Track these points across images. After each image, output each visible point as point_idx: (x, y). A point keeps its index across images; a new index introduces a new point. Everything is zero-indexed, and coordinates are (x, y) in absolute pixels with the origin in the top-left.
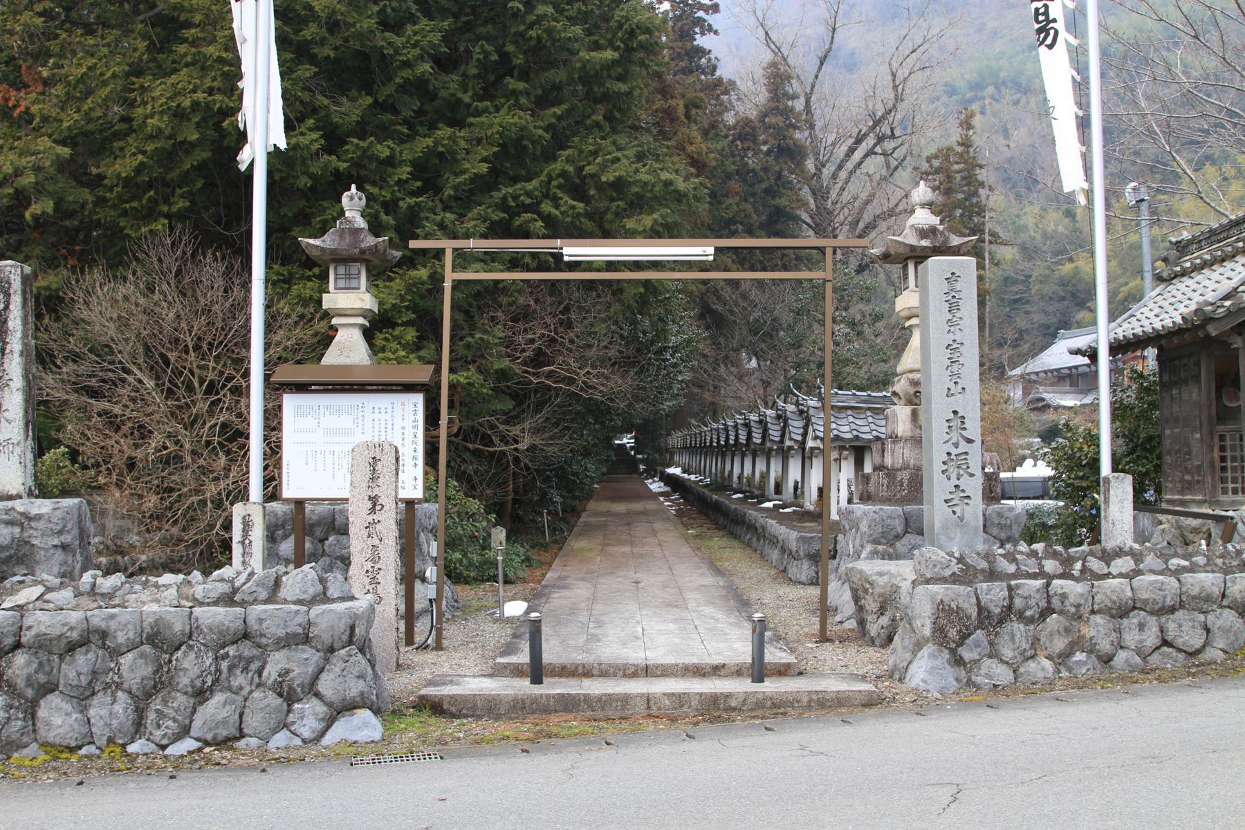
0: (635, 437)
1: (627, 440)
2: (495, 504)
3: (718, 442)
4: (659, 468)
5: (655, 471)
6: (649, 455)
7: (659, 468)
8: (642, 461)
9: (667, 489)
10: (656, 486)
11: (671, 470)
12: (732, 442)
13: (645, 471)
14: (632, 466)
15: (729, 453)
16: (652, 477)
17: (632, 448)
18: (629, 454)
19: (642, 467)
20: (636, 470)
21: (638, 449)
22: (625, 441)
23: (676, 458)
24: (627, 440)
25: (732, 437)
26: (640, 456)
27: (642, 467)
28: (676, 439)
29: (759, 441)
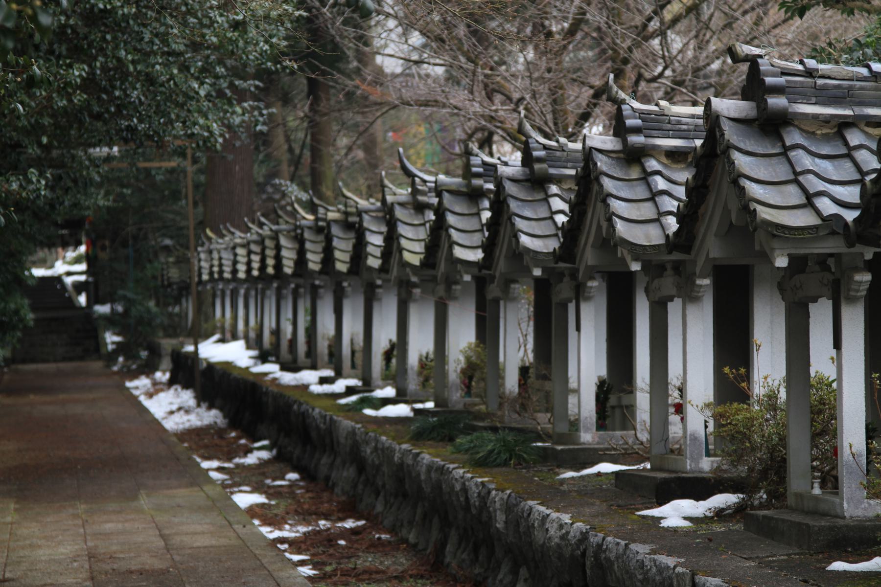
0: (89, 258)
1: (67, 267)
2: (617, 69)
3: (249, 270)
4: (167, 344)
5: (155, 353)
6: (129, 303)
7: (167, 344)
8: (111, 321)
9: (210, 417)
10: (171, 407)
11: (212, 351)
12: (270, 270)
13: (120, 348)
14: (82, 335)
15: (288, 293)
16: (148, 369)
17: (79, 287)
18: (71, 304)
19: (111, 339)
20: (95, 348)
21: (95, 288)
22: (60, 268)
23: (222, 312)
24: (67, 267)
25: (270, 262)
26: (103, 309)
27: (111, 339)
28: (226, 252)
29: (415, 260)
